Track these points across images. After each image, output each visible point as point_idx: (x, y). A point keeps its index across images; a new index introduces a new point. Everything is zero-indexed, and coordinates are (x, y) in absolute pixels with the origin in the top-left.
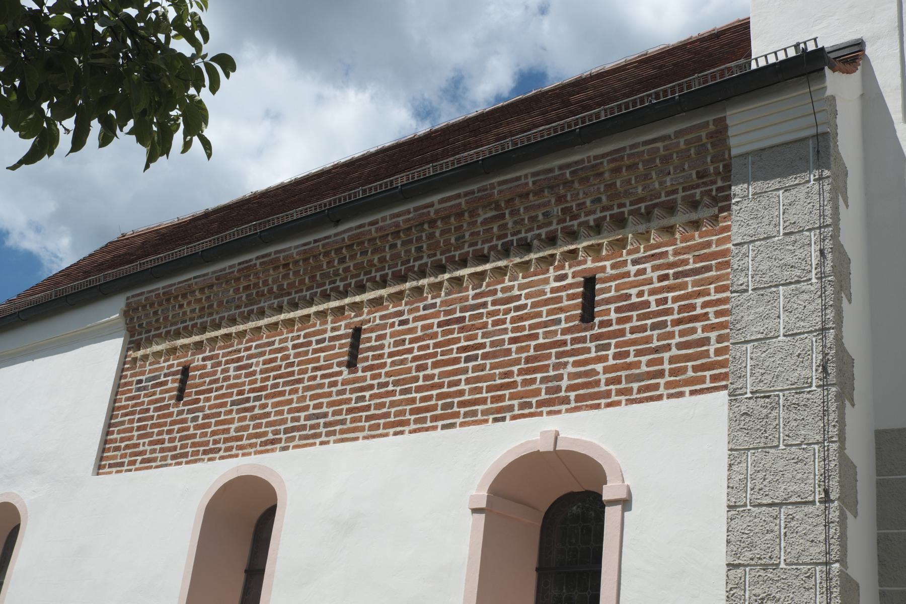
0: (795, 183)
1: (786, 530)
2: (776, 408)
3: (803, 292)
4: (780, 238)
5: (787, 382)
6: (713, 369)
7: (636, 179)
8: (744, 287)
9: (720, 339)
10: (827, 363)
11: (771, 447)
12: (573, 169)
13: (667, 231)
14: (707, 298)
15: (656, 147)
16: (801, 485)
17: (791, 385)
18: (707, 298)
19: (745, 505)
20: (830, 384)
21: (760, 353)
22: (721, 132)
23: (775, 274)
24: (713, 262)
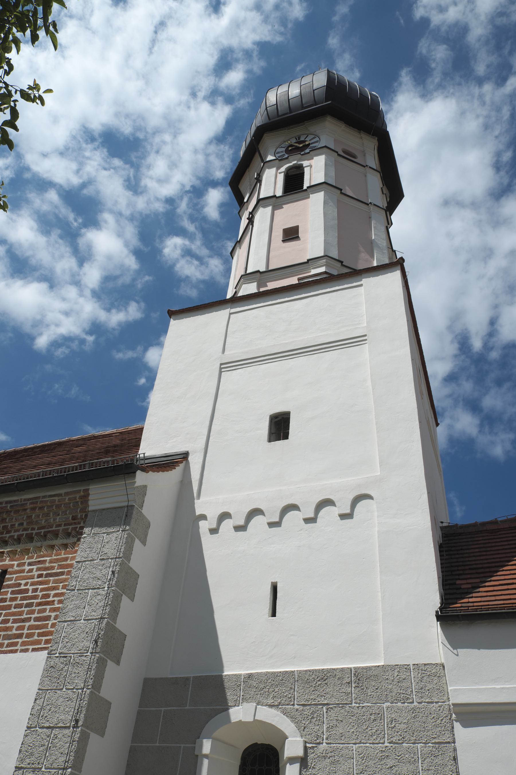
0: (113, 531)
1: (51, 745)
2: (68, 664)
3: (99, 595)
4: (97, 561)
5: (77, 649)
6: (47, 636)
7: (42, 515)
8: (73, 588)
9: (56, 617)
10: (98, 639)
11: (59, 690)
12: (12, 504)
13: (52, 548)
14: (57, 591)
15: (54, 499)
16: (66, 716)
17: (79, 650)
18: (57, 591)
19: (36, 727)
20: (97, 652)
21: (70, 629)
22: (86, 497)
23: (90, 582)
24: (66, 570)
